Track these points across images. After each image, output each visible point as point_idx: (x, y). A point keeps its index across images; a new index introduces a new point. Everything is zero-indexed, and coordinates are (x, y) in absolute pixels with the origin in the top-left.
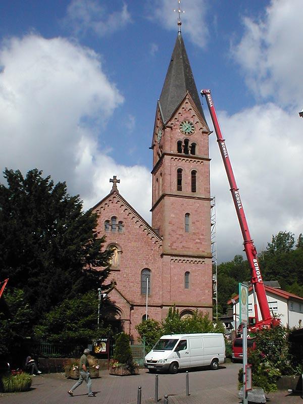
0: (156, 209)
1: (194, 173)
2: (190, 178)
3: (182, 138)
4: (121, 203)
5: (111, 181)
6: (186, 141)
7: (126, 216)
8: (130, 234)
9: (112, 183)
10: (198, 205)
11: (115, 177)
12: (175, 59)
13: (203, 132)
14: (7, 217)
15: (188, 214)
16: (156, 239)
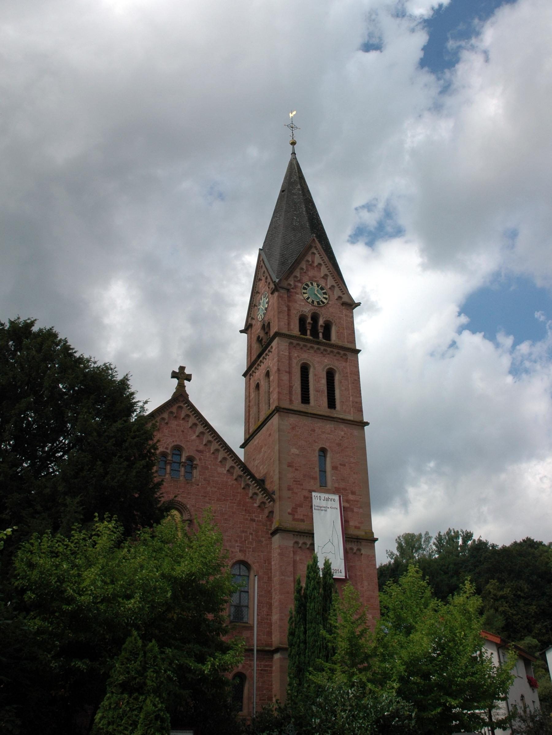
0: (256, 441)
1: (330, 375)
2: (324, 381)
3: (307, 310)
4: (193, 420)
5: (174, 375)
6: (315, 318)
7: (201, 447)
8: (209, 484)
9: (175, 381)
10: (343, 433)
11: (182, 369)
12: (286, 191)
16: (260, 497)
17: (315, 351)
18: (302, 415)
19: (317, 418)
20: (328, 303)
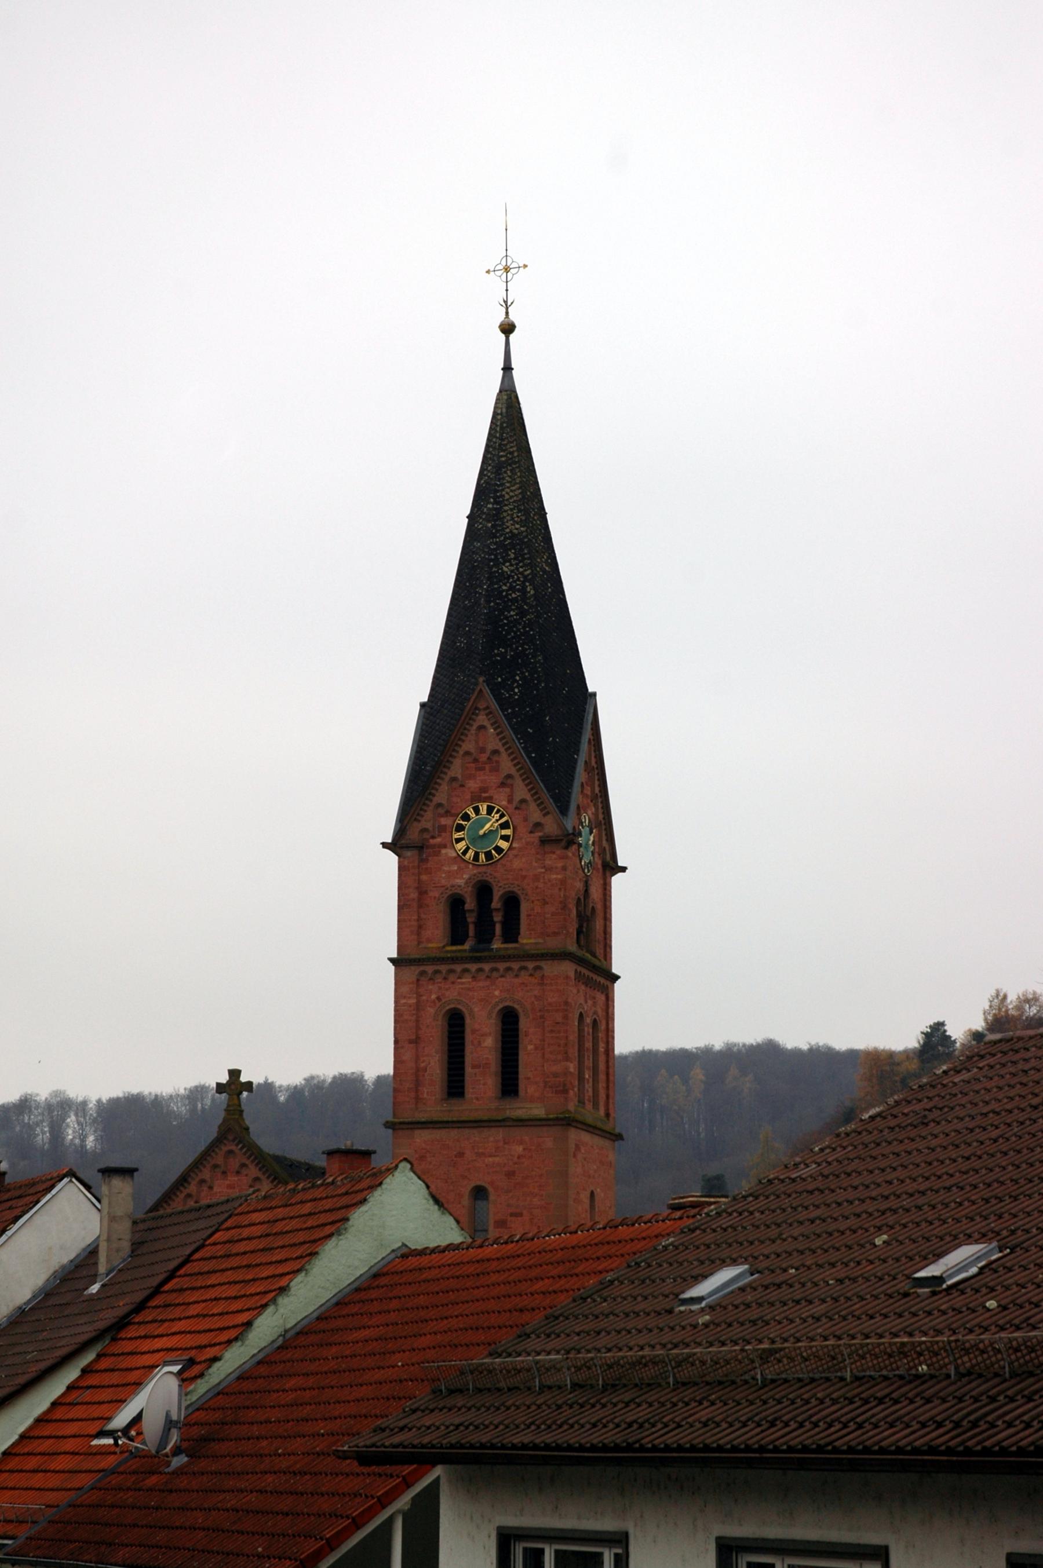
1: (509, 1020)
3: (462, 882)
6: (483, 890)
10: (520, 1149)
13: (544, 841)
14: (231, 1138)
15: (479, 1193)
17: (473, 977)
18: (440, 1128)
19: (468, 1127)
20: (510, 848)
